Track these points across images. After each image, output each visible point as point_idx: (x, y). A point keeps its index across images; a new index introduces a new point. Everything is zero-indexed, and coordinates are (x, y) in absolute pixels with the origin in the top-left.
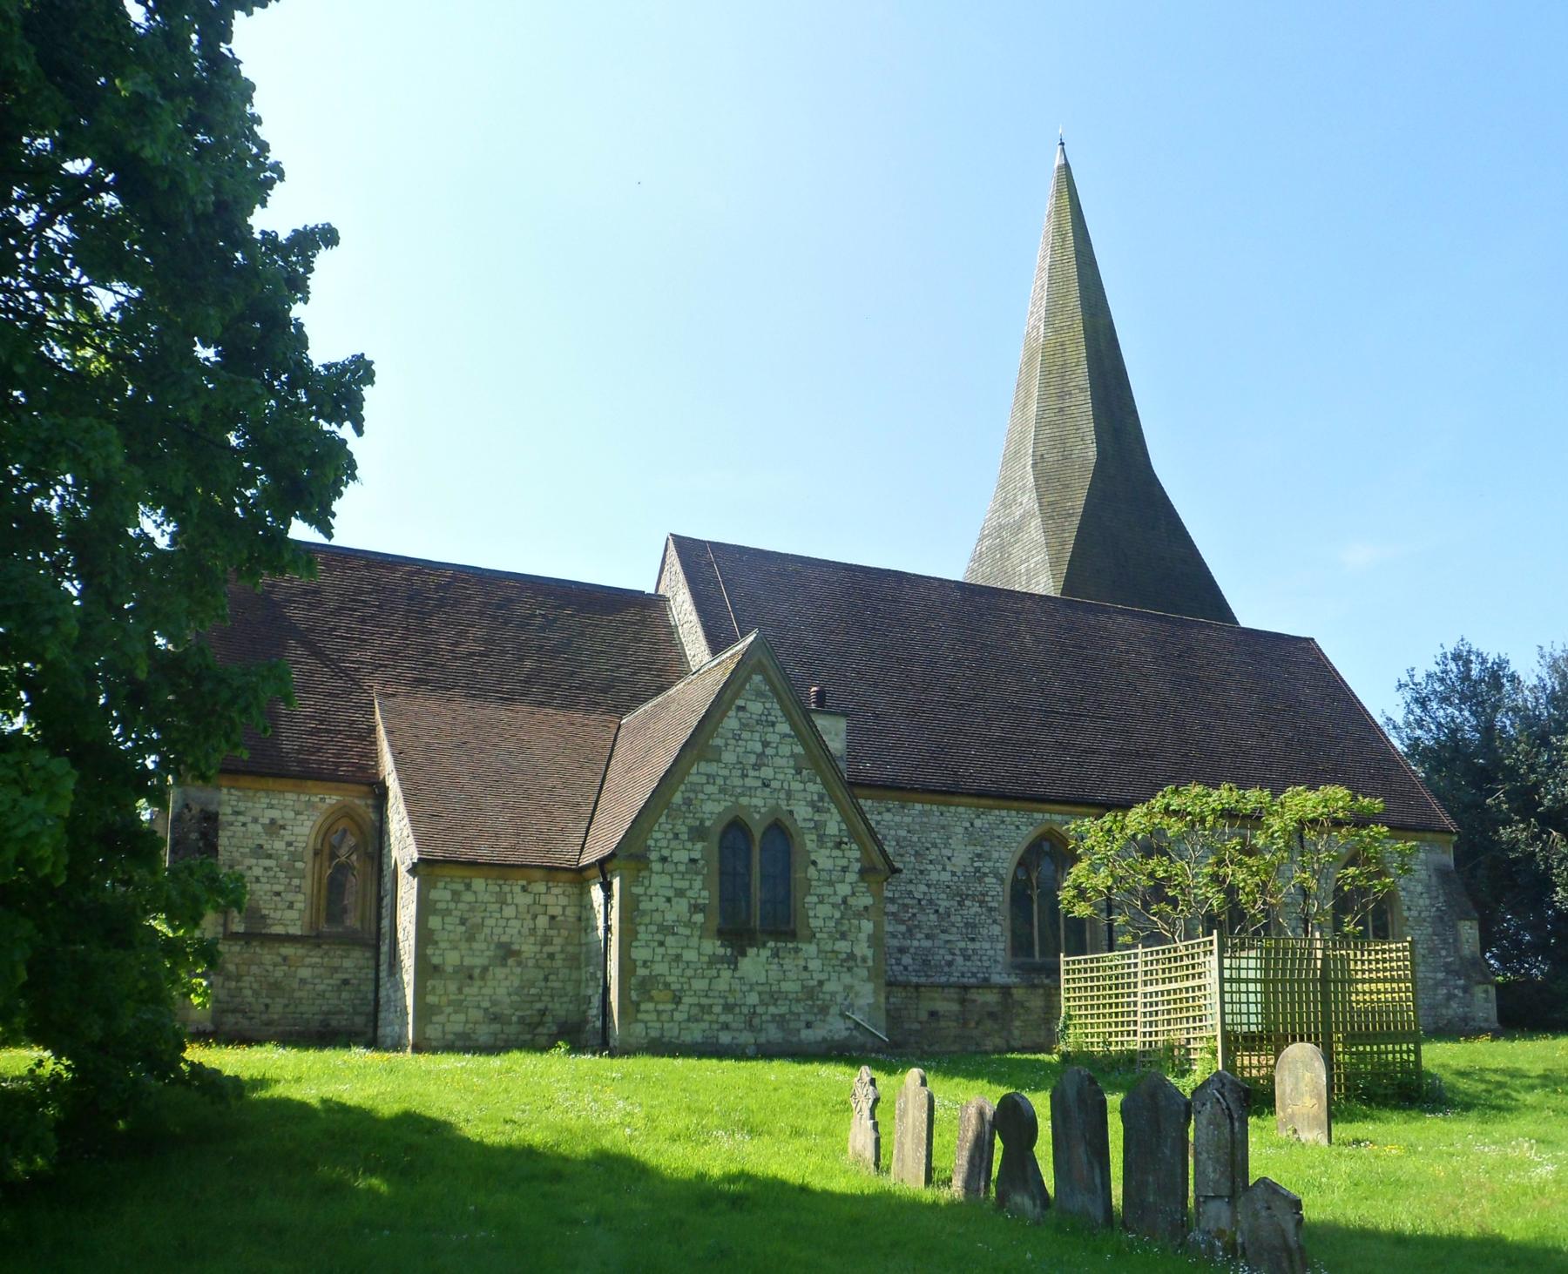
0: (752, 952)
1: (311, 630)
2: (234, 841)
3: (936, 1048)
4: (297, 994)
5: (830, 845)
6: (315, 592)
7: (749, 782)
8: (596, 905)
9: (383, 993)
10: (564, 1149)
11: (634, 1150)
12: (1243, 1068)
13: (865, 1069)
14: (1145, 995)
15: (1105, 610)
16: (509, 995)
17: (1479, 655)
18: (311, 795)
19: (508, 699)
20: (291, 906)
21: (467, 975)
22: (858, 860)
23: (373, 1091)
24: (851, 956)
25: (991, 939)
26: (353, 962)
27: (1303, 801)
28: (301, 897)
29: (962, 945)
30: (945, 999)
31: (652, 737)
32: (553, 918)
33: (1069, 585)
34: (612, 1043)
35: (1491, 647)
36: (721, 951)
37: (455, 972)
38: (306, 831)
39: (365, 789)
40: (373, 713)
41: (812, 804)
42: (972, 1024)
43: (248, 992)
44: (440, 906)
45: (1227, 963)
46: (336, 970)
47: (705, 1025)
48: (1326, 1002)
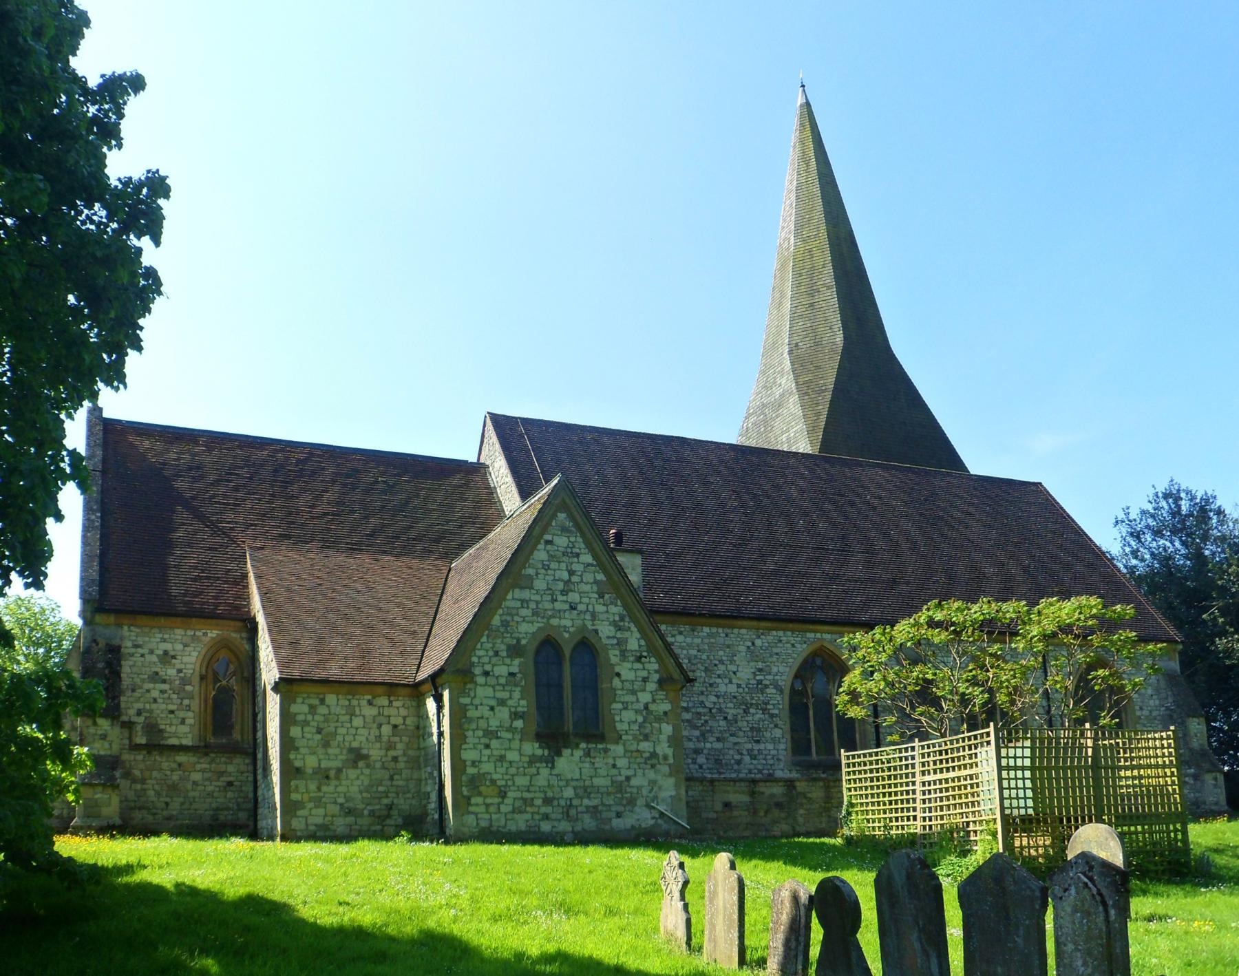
1: (193, 498)
2: (135, 669)
3: (730, 834)
4: (191, 794)
5: (632, 659)
6: (198, 468)
7: (558, 606)
8: (430, 715)
9: (260, 793)
10: (391, 930)
11: (457, 930)
12: (1022, 847)
13: (674, 854)
14: (924, 784)
15: (859, 464)
16: (361, 792)
17: (1188, 492)
18: (195, 630)
19: (355, 549)
20: (183, 722)
22: (656, 672)
23: (222, 876)
24: (654, 755)
25: (774, 741)
26: (235, 767)
27: (1061, 611)
28: (190, 714)
29: (749, 746)
30: (736, 792)
31: (475, 573)
32: (395, 726)
33: (825, 445)
34: (448, 832)
35: (1198, 484)
36: (539, 752)
37: (315, 773)
38: (193, 659)
39: (239, 624)
40: (245, 563)
41: (614, 624)
42: (762, 814)
43: (151, 793)
44: (300, 718)
45: (1003, 752)
46: (222, 774)
47: (528, 816)
48: (1097, 786)
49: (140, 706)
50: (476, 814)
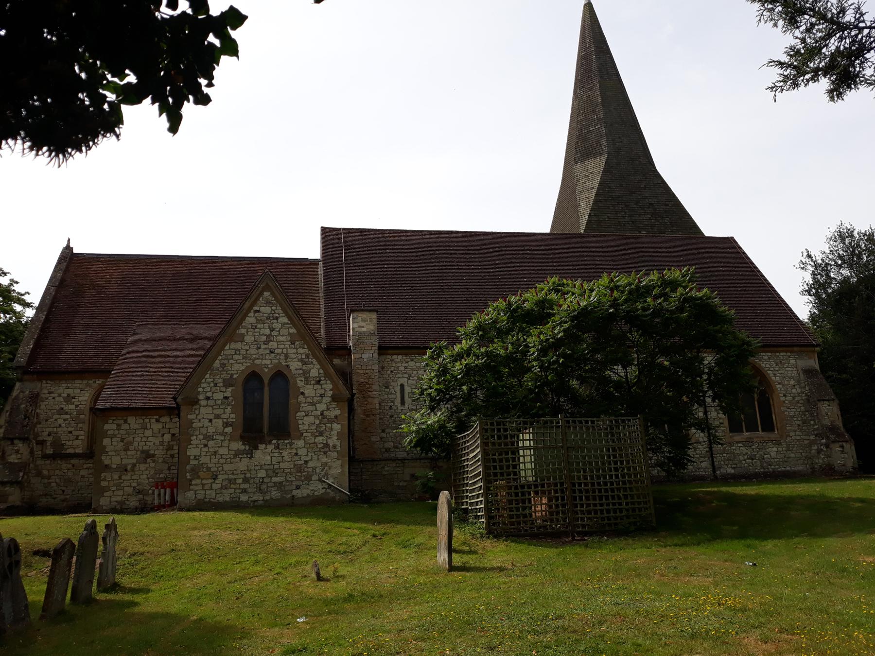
0: (262, 447)
24: (326, 445)
28: (82, 433)
32: (173, 435)
41: (301, 360)
43: (54, 484)
44: (109, 432)
47: (232, 491)
49: (51, 430)
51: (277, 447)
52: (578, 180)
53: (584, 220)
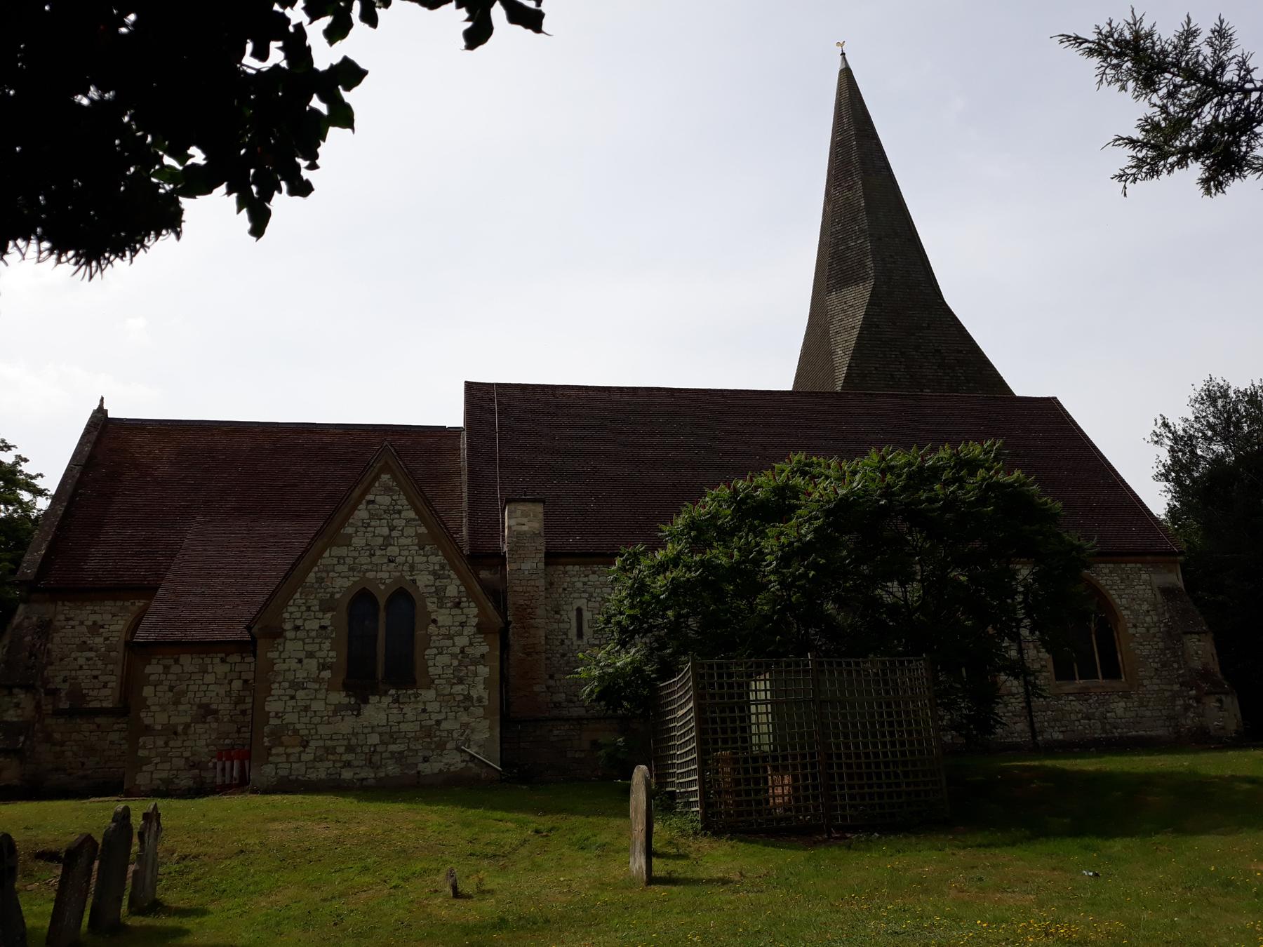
0: (374, 699)
21: (172, 731)
24: (468, 698)
32: (246, 681)
41: (434, 573)
43: (69, 754)
47: (330, 764)
50: (277, 764)
51: (396, 700)
52: (833, 317)
53: (841, 373)
